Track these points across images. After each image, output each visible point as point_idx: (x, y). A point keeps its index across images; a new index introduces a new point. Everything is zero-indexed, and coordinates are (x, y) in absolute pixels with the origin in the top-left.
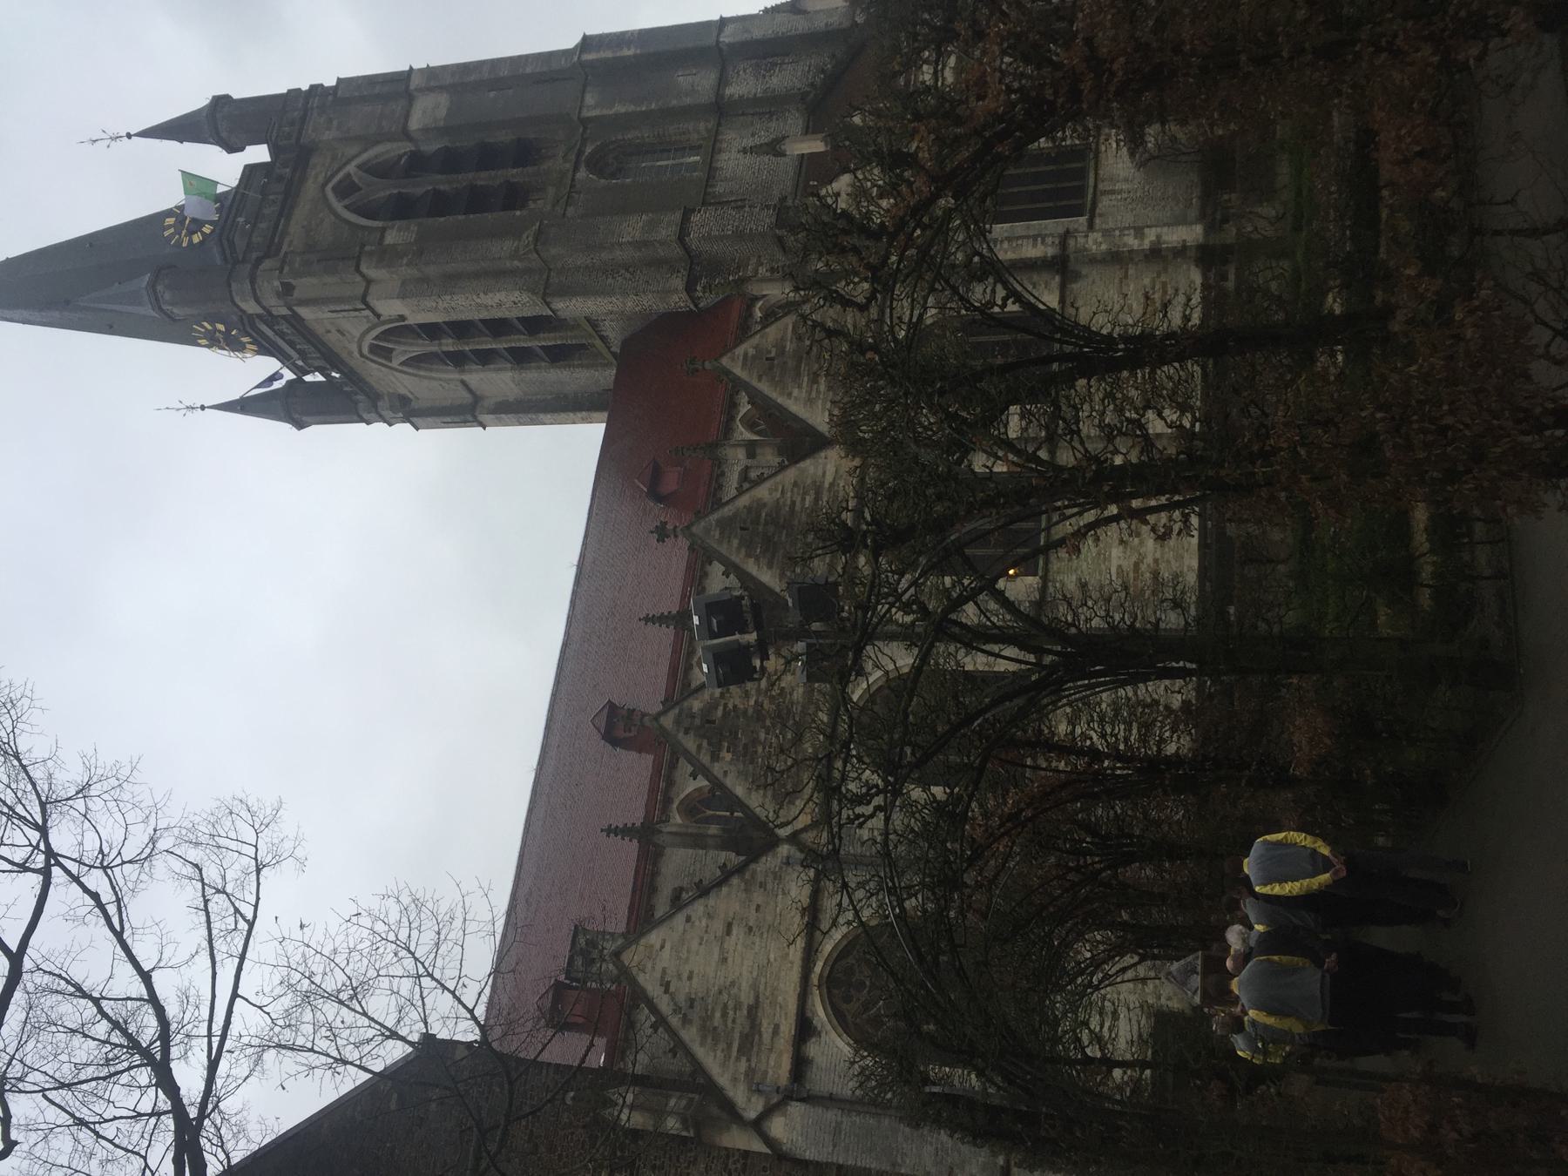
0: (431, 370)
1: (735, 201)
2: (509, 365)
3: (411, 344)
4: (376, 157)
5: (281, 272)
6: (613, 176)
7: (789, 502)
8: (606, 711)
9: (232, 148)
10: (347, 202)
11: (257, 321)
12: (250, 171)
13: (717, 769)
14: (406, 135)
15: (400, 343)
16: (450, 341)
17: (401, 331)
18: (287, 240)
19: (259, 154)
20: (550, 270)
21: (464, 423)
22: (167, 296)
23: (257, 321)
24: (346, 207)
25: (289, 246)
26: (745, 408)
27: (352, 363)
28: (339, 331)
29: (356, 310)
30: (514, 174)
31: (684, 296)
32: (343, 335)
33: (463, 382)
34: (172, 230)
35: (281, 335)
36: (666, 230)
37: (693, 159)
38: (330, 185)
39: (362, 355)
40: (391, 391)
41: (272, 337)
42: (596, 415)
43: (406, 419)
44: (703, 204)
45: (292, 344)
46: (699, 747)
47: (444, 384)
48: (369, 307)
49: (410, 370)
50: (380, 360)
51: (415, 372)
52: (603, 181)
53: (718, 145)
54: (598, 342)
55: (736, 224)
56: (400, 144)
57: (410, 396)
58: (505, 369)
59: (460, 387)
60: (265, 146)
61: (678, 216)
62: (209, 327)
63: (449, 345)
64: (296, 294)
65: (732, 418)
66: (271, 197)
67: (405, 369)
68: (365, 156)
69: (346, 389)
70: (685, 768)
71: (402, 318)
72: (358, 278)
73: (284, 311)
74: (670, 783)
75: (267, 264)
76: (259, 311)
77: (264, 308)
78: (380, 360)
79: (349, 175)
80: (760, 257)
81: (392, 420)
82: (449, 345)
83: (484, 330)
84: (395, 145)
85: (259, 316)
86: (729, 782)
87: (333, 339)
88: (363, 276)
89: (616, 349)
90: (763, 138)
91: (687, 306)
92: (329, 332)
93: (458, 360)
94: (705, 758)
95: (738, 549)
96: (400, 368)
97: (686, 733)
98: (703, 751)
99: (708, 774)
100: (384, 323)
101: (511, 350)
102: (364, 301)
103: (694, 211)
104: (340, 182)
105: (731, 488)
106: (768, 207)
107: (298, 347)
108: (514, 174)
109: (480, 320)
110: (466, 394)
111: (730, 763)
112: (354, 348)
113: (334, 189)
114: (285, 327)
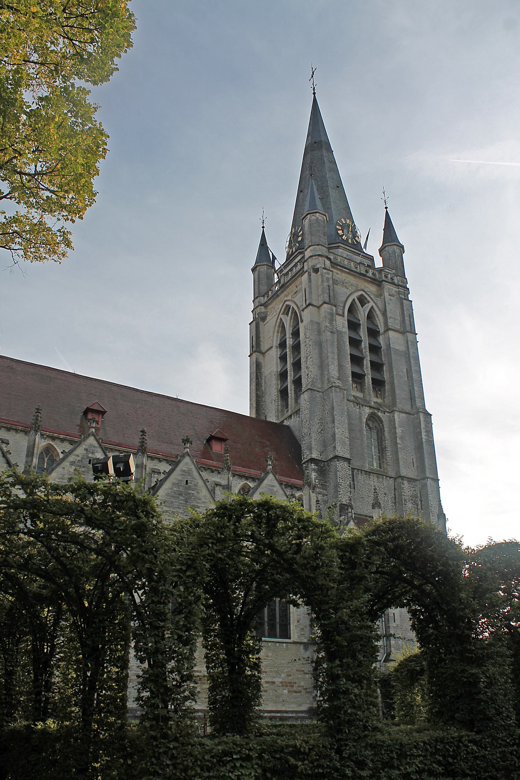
0: (278, 332)
1: (354, 485)
2: (279, 370)
3: (290, 324)
4: (377, 315)
5: (323, 268)
6: (367, 424)
7: (199, 505)
8: (102, 410)
9: (381, 251)
10: (356, 299)
11: (302, 255)
12: (371, 259)
13: (66, 464)
14: (387, 329)
15: (291, 319)
16: (291, 343)
17: (296, 320)
18: (339, 272)
19: (379, 263)
20: (323, 392)
21: (252, 347)
22: (313, 218)
23: (302, 255)
24: (354, 300)
25: (336, 273)
26: (252, 485)
27: (282, 296)
28: (296, 292)
29: (306, 300)
30: (368, 380)
31: (309, 458)
32: (295, 293)
33: (272, 347)
34: (344, 222)
35: (295, 265)
36: (342, 451)
37: (375, 464)
38: (364, 293)
39: (285, 301)
40: (268, 313)
41: (294, 261)
42: (254, 411)
43: (255, 319)
44: (353, 469)
45: (291, 270)
46: (78, 456)
47: (271, 338)
48: (307, 306)
49: (278, 323)
50: (283, 309)
51: (277, 325)
52: (365, 420)
53: (381, 476)
54: (289, 413)
55: (343, 484)
56: (383, 326)
57: (266, 322)
58: (277, 368)
59: (269, 346)
60: (382, 266)
61: (348, 456)
62: (300, 234)
63: (289, 342)
64: (313, 274)
65: (247, 478)
66: (358, 266)
67: (279, 320)
68: (378, 312)
69: (270, 292)
70: (67, 447)
71: (302, 321)
72: (320, 303)
73: (306, 268)
74: (63, 440)
75: (328, 263)
76: (306, 257)
77: (308, 259)
78: (283, 309)
79: (369, 302)
80: (327, 495)
81: (254, 312)
82: (289, 342)
83: (296, 359)
84: (382, 324)
85: (303, 257)
86: (59, 469)
87: (292, 288)
88: (321, 305)
89: (286, 423)
90: (381, 498)
91: (304, 458)
92: (297, 287)
93: (283, 345)
94: (71, 458)
95: (176, 479)
96: (279, 318)
97: (86, 450)
98: (75, 457)
99: (63, 459)
100: (300, 313)
101: (286, 372)
102: (309, 304)
103: (349, 464)
104: (365, 298)
105: (205, 475)
106: (350, 500)
107: (290, 273)
108: (368, 380)
109: (300, 358)
110: (266, 348)
111: (68, 471)
112: (289, 298)
113: (362, 295)
114: (299, 267)
